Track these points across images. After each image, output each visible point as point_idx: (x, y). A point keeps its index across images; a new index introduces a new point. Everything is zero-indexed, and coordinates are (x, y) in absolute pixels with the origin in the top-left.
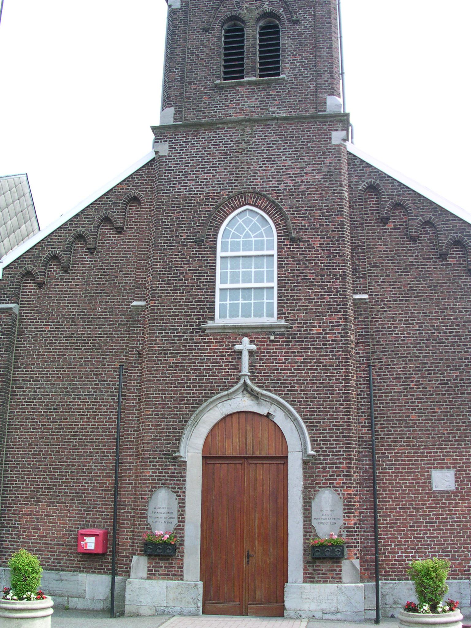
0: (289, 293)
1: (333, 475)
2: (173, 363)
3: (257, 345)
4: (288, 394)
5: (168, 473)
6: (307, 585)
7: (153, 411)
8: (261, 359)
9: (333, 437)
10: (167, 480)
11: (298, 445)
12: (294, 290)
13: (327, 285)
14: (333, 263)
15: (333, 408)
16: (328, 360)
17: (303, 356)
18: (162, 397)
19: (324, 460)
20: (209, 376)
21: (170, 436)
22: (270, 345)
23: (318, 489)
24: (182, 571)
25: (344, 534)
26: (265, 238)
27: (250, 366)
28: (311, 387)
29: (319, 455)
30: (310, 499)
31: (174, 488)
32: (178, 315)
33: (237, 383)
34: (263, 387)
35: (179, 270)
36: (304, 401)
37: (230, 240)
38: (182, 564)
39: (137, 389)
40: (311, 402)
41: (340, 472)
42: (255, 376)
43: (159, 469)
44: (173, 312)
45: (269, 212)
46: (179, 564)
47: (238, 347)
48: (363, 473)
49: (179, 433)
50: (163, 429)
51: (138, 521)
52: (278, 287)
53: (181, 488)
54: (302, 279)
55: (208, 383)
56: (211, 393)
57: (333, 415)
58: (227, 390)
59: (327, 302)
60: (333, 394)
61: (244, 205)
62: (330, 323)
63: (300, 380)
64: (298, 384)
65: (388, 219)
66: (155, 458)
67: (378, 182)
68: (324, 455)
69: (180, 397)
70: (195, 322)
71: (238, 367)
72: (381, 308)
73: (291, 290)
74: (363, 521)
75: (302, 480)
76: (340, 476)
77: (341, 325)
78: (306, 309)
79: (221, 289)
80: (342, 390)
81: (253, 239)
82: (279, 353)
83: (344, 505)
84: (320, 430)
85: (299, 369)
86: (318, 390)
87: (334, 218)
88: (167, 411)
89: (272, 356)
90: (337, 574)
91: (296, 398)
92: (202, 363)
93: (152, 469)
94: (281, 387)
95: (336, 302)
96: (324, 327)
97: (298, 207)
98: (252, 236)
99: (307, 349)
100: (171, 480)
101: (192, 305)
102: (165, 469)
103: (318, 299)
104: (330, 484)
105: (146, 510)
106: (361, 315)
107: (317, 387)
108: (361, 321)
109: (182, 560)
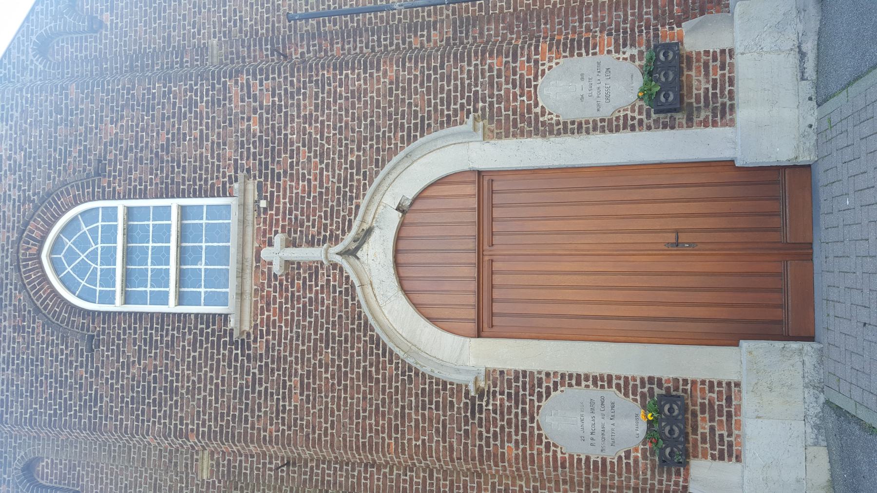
0: (190, 175)
1: (514, 81)
2: (302, 394)
3: (276, 232)
4: (365, 173)
5: (509, 408)
6: (742, 115)
7: (390, 438)
8: (302, 226)
9: (442, 87)
10: (523, 410)
11: (461, 151)
12: (184, 167)
13: (180, 108)
14: (143, 100)
15: (391, 89)
16: (307, 102)
17: (298, 148)
18: (364, 418)
19: (484, 101)
20: (328, 323)
21: (437, 403)
22: (278, 209)
23: (538, 110)
24: (720, 384)
25: (629, 51)
26: (100, 224)
27: (313, 245)
28: (353, 131)
29: (476, 110)
30: (558, 123)
31: (540, 395)
32: (217, 385)
33: (341, 269)
34: (350, 221)
35: (139, 382)
36: (378, 143)
37: (98, 289)
38: (703, 382)
39: (353, 470)
40: (378, 130)
41: (507, 69)
42: (331, 235)
43: (502, 427)
44: (210, 395)
45: (53, 215)
46: (702, 390)
47: (277, 269)
48: (512, 33)
49: (431, 383)
50: (423, 415)
51: (612, 478)
52: (178, 197)
53: (540, 380)
54: (167, 153)
55: (340, 325)
56: (360, 318)
57: (403, 88)
58: (353, 287)
59: (207, 107)
60: (366, 90)
61: (40, 263)
62: (243, 100)
63: (340, 151)
64: (346, 155)
65: (92, 19)
66: (481, 434)
67: (34, 38)
68: (476, 101)
69: (364, 380)
70: (231, 352)
71: (314, 269)
72: (235, 26)
73: (184, 172)
74: (603, 24)
75: (523, 140)
76: (514, 68)
77: (248, 80)
78: (218, 144)
79: (126, 302)
80: (359, 74)
81: (99, 245)
82: (291, 192)
83: (572, 55)
84: (429, 111)
85: (322, 155)
86: (359, 119)
87: (72, 100)
88: (390, 409)
89: (297, 204)
90: (715, 59)
91: (371, 158)
92: (303, 337)
93: (502, 442)
94: (351, 186)
95: (207, 90)
96: (249, 112)
97: (50, 163)
98: (94, 247)
99: (286, 140)
100: (524, 403)
101: (200, 359)
102: (502, 413)
103: (201, 125)
104: (529, 86)
105: (588, 458)
106: (238, 53)
107: (353, 120)
108: (249, 52)
109: (694, 383)
